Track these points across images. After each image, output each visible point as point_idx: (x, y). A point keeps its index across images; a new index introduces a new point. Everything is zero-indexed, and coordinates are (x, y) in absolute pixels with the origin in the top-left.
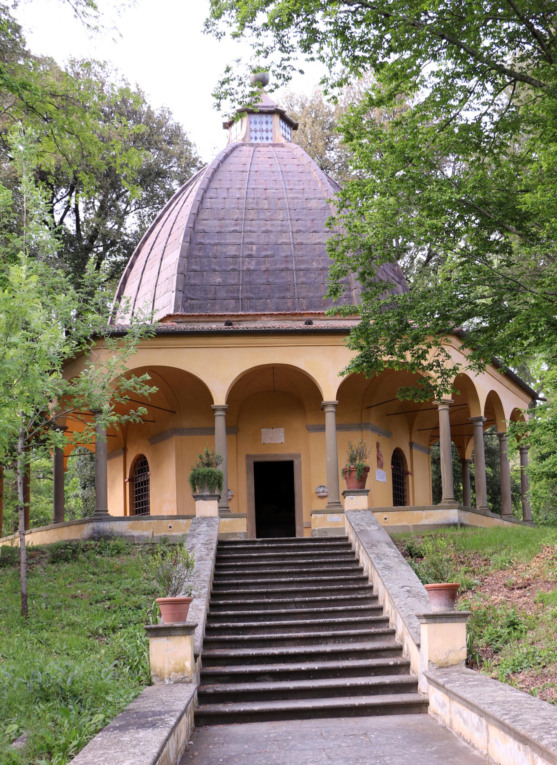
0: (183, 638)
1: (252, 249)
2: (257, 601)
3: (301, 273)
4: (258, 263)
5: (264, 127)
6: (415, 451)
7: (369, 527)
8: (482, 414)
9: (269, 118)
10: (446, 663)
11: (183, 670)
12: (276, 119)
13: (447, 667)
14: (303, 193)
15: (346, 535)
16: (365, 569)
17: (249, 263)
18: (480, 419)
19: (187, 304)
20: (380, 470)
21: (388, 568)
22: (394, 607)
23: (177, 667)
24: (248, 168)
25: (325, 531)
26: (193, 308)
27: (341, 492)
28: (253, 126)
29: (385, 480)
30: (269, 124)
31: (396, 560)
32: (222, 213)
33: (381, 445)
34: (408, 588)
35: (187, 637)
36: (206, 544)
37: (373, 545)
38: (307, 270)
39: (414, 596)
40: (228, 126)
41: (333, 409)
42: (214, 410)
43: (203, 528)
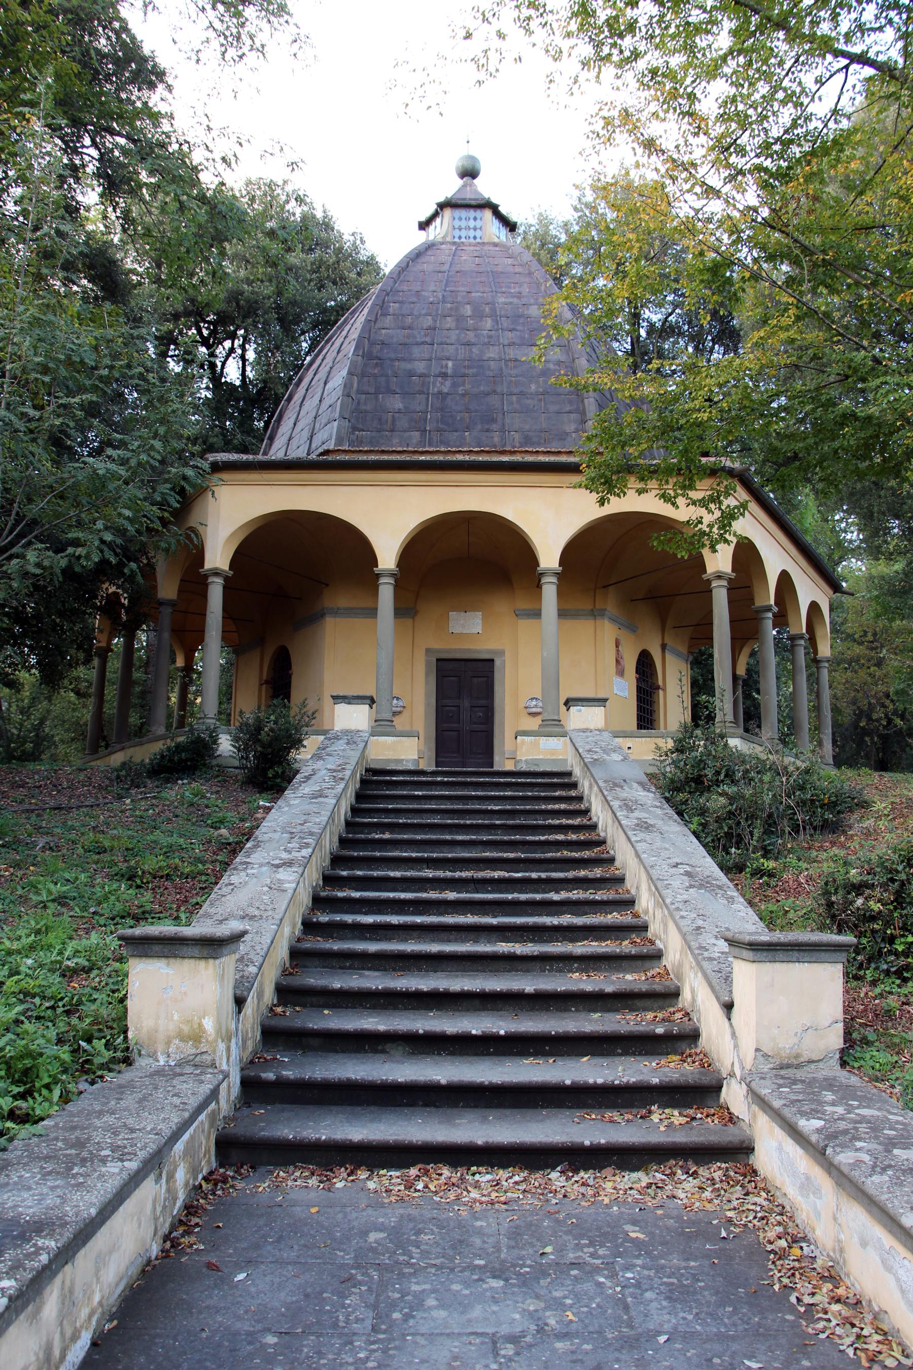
0: (202, 963)
1: (446, 366)
2: (408, 874)
3: (514, 398)
4: (454, 385)
5: (472, 224)
6: (668, 656)
7: (608, 755)
8: (772, 602)
9: (478, 213)
10: (797, 1056)
11: (196, 1037)
12: (488, 214)
13: (798, 1066)
14: (519, 298)
15: (569, 769)
16: (600, 826)
17: (442, 384)
18: (768, 609)
19: (353, 437)
20: (619, 679)
21: (644, 826)
22: (661, 901)
23: (186, 1029)
24: (446, 268)
25: (536, 762)
26: (362, 442)
27: (563, 701)
28: (457, 223)
29: (626, 694)
30: (478, 221)
31: (659, 811)
32: (409, 320)
33: (622, 642)
34: (688, 869)
35: (211, 961)
36: (335, 771)
37: (615, 785)
38: (522, 393)
39: (701, 887)
40: (424, 225)
41: (554, 580)
42: (378, 576)
43: (340, 745)
